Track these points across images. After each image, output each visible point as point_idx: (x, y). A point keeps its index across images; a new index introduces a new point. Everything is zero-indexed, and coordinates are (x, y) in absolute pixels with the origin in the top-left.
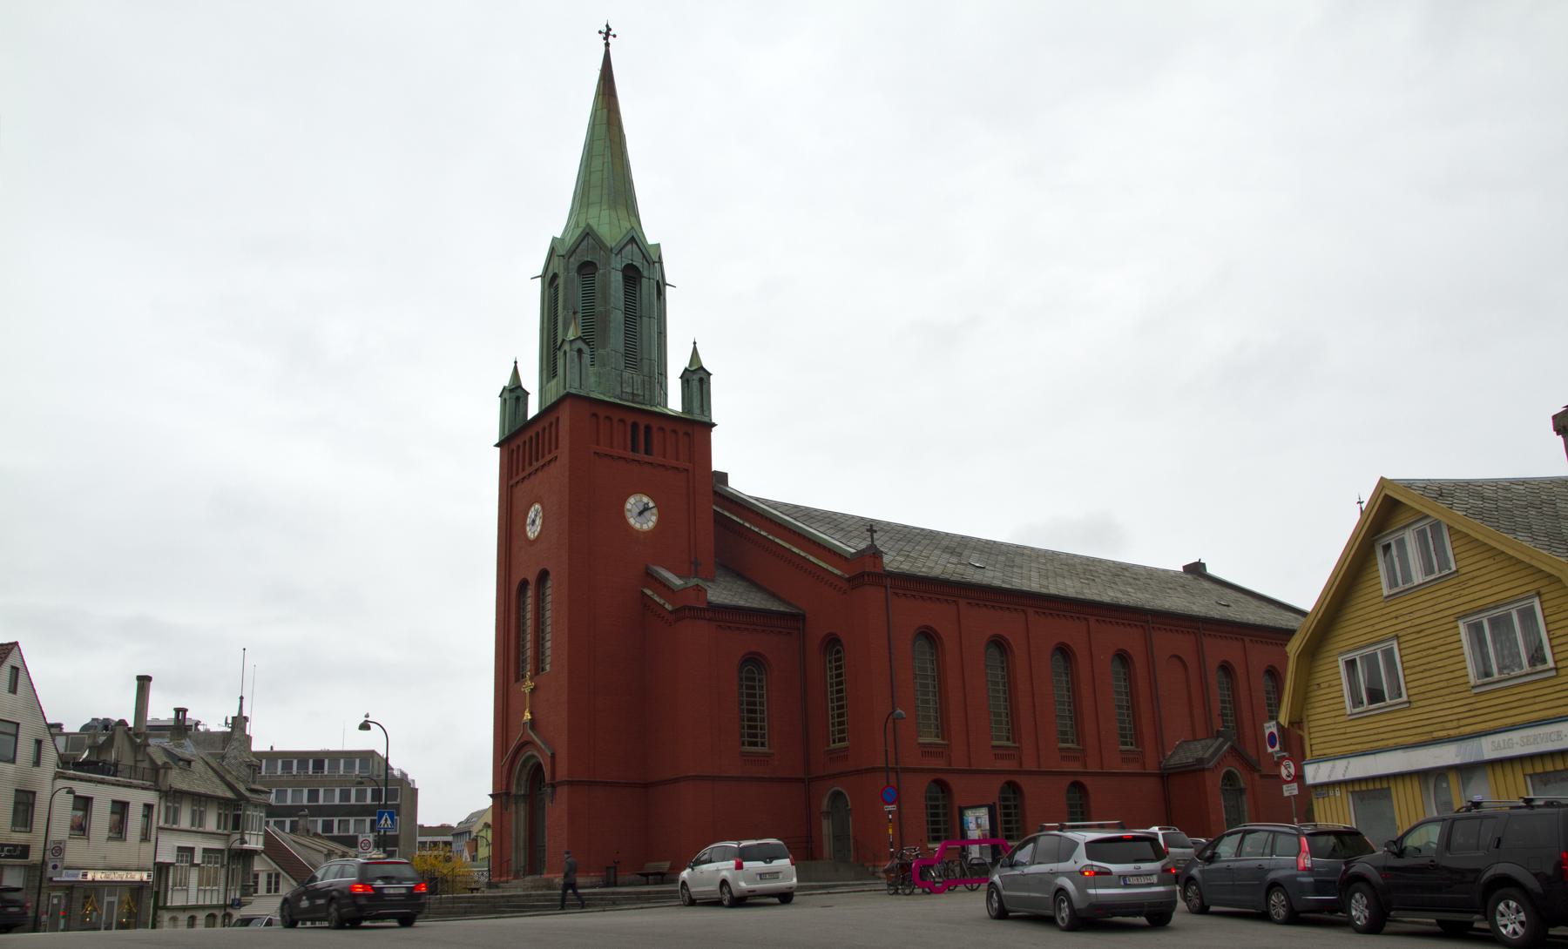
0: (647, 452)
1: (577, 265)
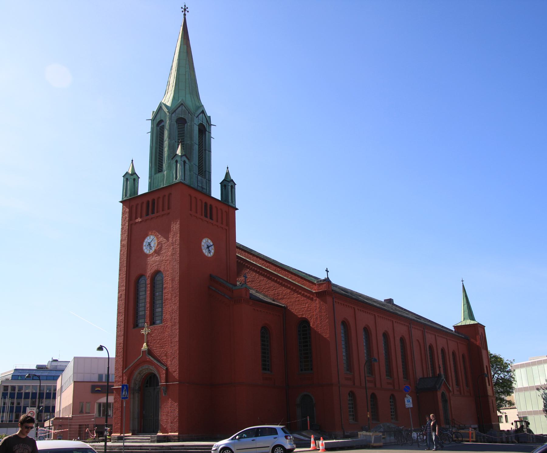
1: (176, 118)
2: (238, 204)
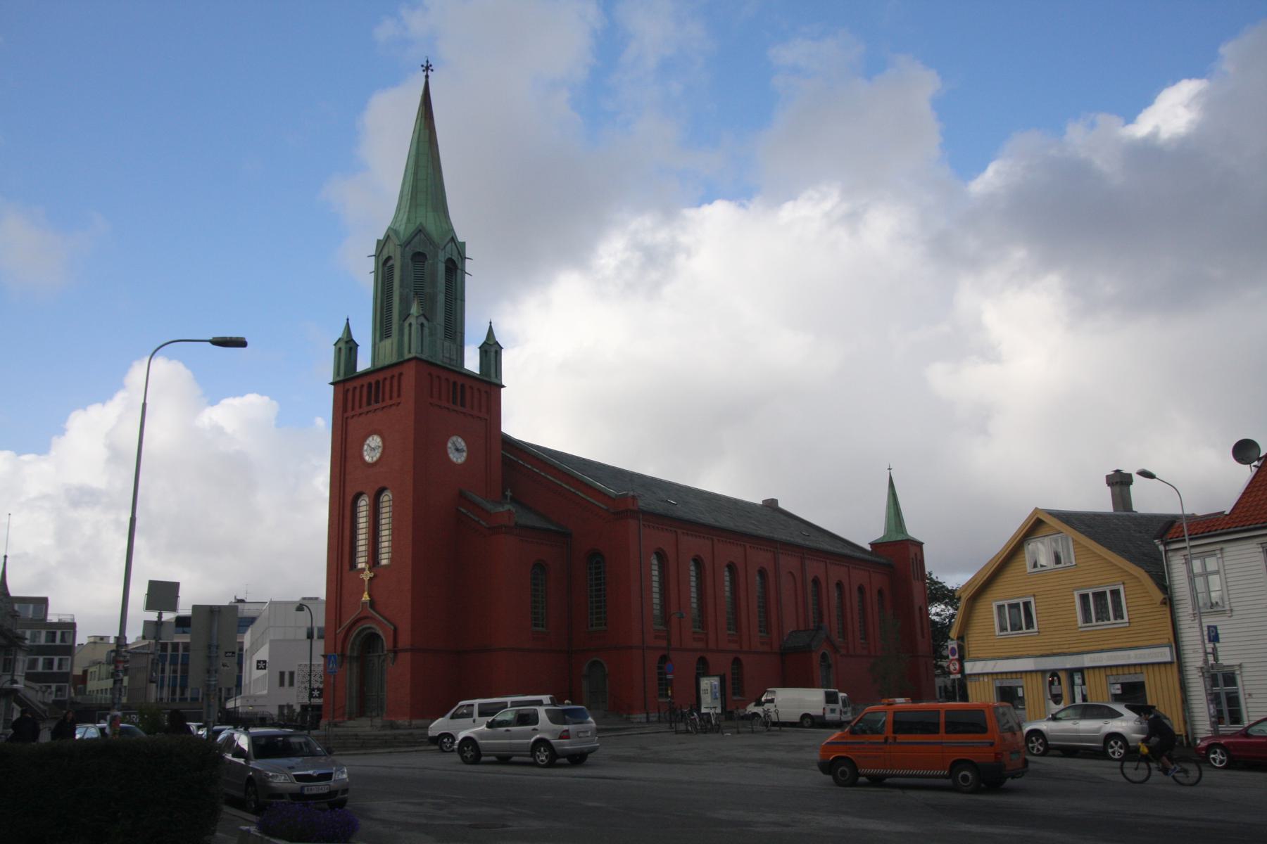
0: (463, 405)
2: (506, 378)
